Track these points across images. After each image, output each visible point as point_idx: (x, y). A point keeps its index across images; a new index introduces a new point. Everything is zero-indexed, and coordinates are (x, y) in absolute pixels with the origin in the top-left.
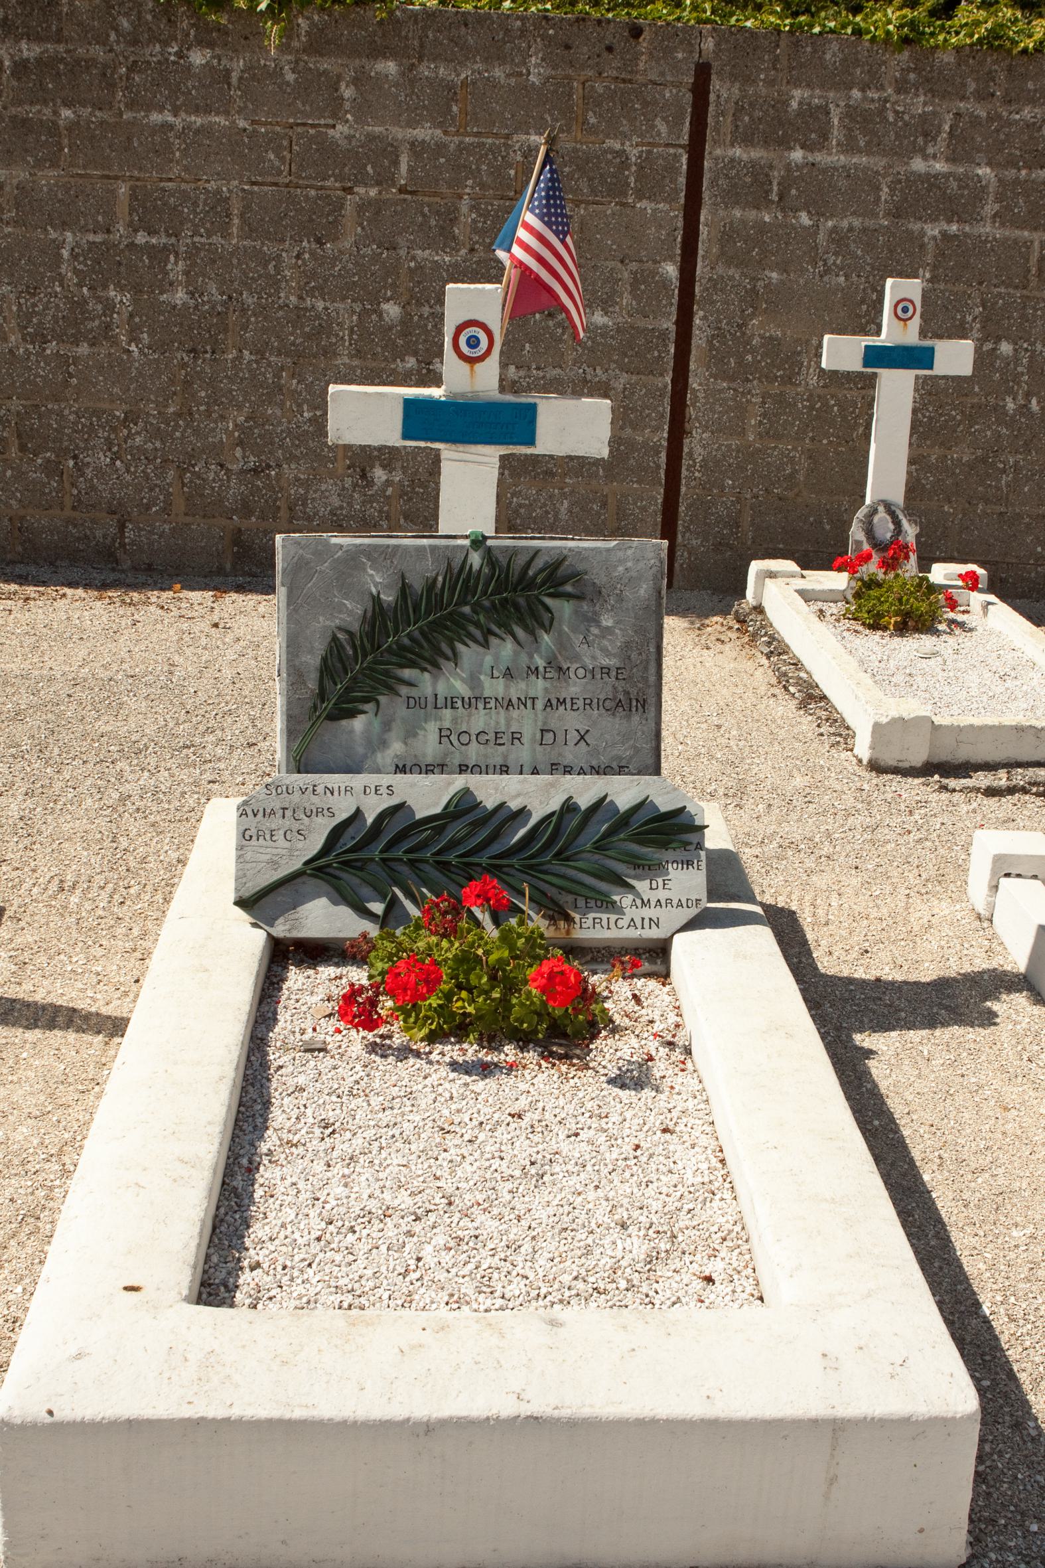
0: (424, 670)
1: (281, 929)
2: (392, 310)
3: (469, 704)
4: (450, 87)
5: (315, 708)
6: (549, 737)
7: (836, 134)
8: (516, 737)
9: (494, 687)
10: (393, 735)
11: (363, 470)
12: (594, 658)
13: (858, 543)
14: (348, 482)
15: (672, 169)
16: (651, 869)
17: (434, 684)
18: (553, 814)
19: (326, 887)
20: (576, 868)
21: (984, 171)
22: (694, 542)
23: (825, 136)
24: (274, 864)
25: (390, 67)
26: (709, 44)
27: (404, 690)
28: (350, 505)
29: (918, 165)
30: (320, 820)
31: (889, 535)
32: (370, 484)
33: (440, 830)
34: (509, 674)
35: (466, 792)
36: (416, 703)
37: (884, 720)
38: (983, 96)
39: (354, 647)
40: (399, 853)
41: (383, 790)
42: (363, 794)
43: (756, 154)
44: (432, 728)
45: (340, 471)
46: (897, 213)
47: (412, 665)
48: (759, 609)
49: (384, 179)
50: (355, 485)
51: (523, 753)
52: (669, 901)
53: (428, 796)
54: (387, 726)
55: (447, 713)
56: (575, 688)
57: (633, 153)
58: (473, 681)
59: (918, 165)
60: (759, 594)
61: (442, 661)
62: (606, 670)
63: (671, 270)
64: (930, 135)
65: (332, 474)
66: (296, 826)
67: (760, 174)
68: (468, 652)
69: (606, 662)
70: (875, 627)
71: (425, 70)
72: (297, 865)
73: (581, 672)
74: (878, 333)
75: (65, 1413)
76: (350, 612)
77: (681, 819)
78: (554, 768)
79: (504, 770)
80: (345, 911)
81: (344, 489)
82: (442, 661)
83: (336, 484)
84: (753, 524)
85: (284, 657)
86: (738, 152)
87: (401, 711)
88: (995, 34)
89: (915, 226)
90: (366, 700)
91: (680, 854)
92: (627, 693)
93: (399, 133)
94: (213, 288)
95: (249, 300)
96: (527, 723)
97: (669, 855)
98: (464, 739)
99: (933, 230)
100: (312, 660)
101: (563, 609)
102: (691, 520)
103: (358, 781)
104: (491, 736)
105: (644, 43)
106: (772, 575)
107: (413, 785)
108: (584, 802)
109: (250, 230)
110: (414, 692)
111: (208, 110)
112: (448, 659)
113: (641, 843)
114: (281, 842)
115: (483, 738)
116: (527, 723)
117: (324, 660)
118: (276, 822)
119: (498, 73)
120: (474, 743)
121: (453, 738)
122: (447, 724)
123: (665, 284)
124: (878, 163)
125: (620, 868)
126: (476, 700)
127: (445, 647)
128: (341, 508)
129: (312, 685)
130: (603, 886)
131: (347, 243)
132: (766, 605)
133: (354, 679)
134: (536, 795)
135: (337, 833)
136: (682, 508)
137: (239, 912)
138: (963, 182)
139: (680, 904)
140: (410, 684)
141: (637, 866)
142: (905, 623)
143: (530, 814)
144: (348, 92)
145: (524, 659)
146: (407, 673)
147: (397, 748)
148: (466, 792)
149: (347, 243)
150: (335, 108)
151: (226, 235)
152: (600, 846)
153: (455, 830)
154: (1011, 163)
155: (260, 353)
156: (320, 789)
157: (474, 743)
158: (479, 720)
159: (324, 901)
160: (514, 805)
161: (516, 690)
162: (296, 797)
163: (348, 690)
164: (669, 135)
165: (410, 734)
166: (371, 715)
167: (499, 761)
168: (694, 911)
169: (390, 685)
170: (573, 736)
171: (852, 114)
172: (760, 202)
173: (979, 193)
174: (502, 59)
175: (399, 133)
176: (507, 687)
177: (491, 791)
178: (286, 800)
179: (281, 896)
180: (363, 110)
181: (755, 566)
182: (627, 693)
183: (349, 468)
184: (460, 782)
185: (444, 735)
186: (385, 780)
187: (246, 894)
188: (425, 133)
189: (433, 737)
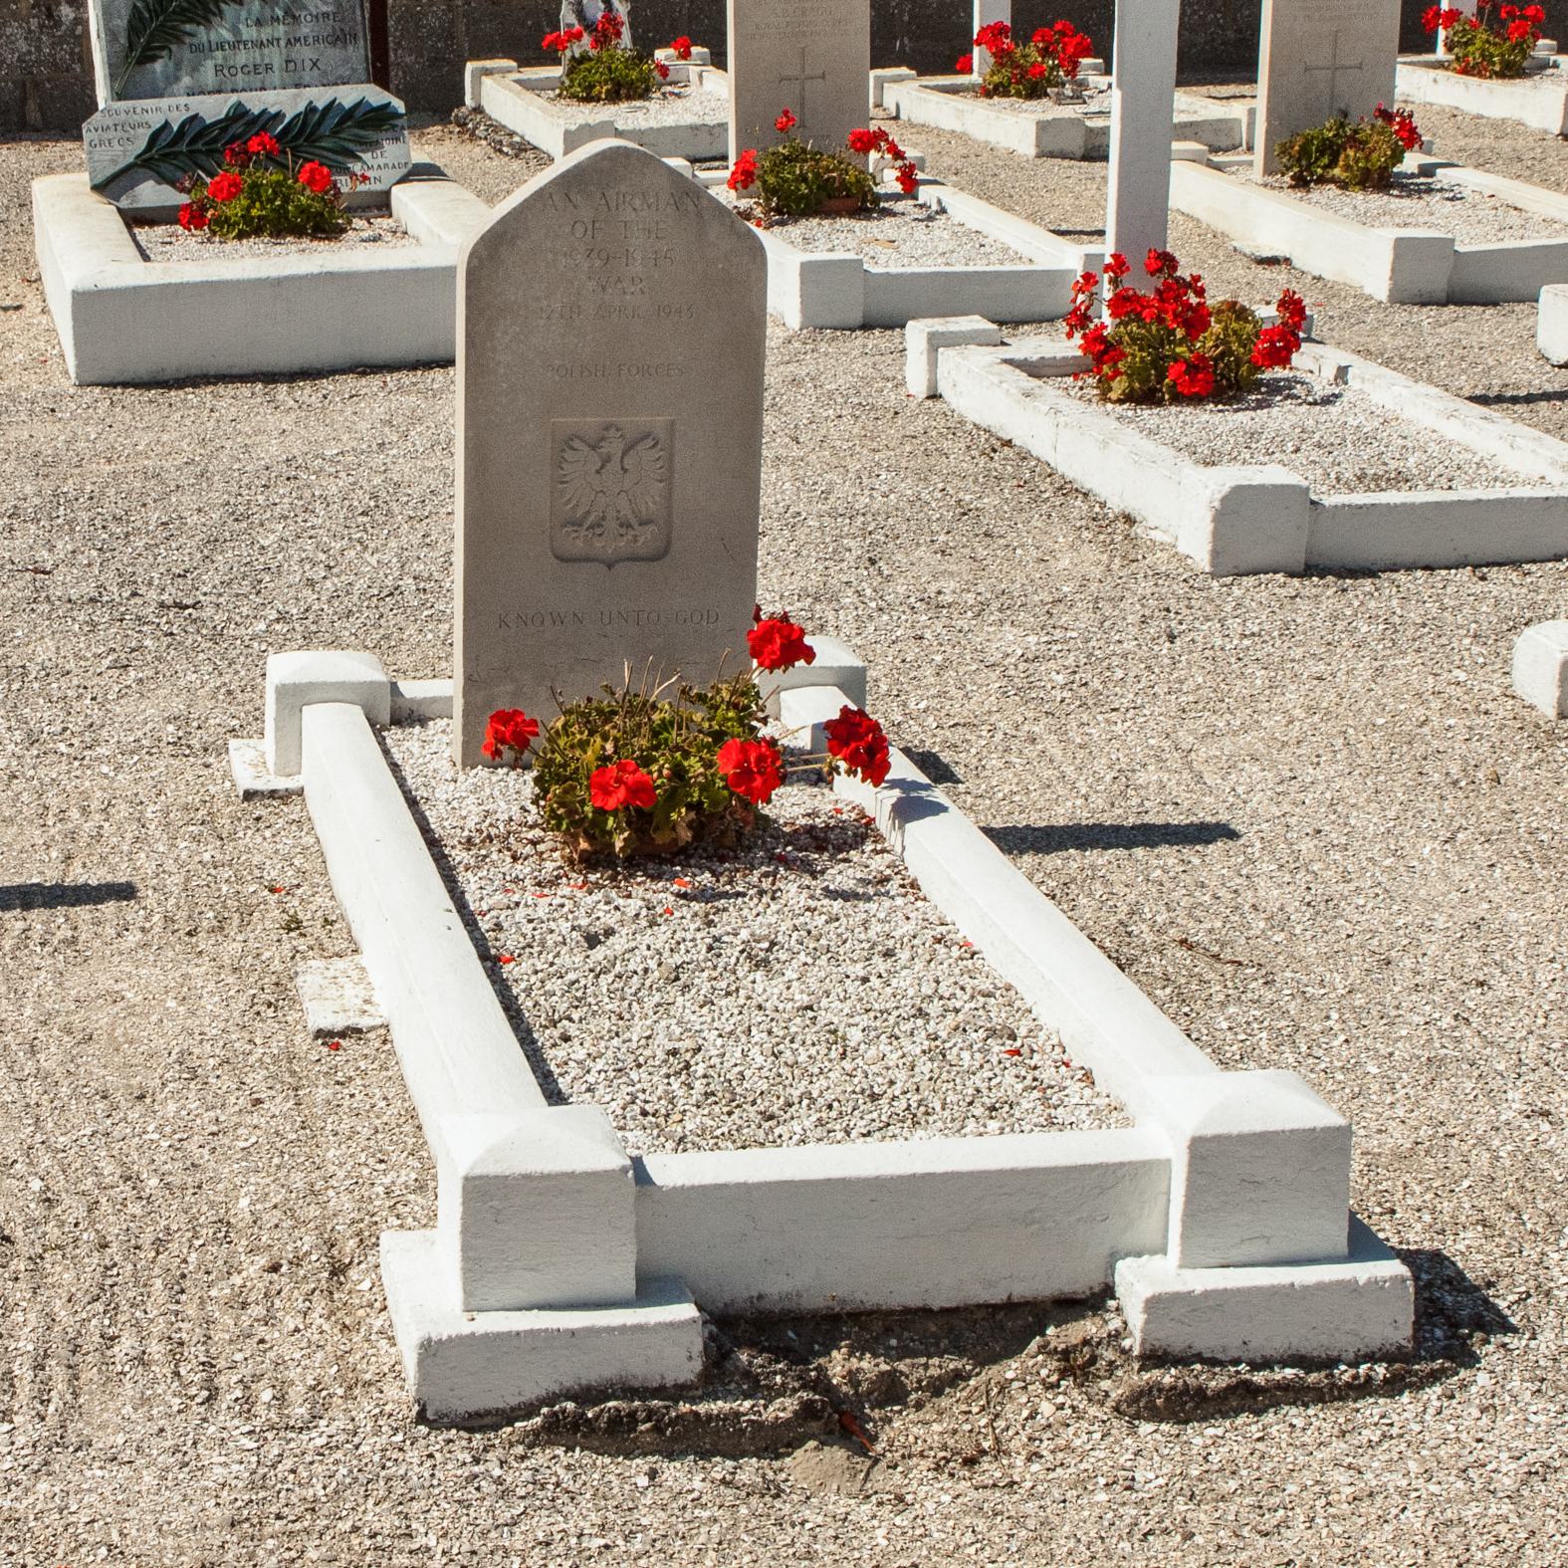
0: (199, 24)
1: (124, 203)
3: (234, 46)
5: (127, 57)
6: (291, 66)
8: (269, 68)
9: (249, 33)
10: (183, 72)
11: (49, 9)
12: (317, 7)
13: (569, 25)
14: (34, 23)
16: (373, 145)
17: (208, 34)
18: (299, 115)
19: (151, 173)
20: (323, 148)
22: (408, 60)
24: (114, 161)
27: (188, 40)
28: (39, 49)
30: (141, 130)
31: (600, 15)
32: (58, 23)
33: (224, 130)
34: (259, 23)
35: (239, 104)
36: (198, 49)
37: (573, 128)
39: (149, 11)
40: (199, 146)
41: (182, 107)
42: (169, 110)
44: (210, 64)
45: (24, 12)
47: (191, 21)
48: (478, 110)
50: (41, 26)
51: (276, 77)
52: (386, 165)
53: (213, 108)
54: (178, 66)
55: (219, 54)
56: (305, 30)
58: (235, 30)
60: (477, 95)
61: (212, 18)
62: (326, 15)
65: (15, 16)
66: (126, 135)
69: (325, 9)
70: (588, 99)
72: (131, 160)
73: (309, 18)
74: (970, 71)
75: (102, 285)
77: (389, 110)
78: (297, 86)
79: (263, 89)
80: (166, 188)
81: (30, 31)
82: (212, 18)
83: (21, 26)
84: (467, 34)
85: (101, 22)
87: (187, 55)
90: (162, 48)
91: (390, 134)
92: (342, 30)
96: (275, 56)
97: (383, 135)
98: (233, 71)
100: (121, 23)
102: (402, 35)
103: (164, 103)
104: (251, 68)
106: (488, 72)
107: (202, 102)
108: (320, 105)
110: (195, 41)
112: (214, 14)
113: (362, 128)
114: (117, 147)
115: (246, 70)
117: (129, 22)
118: (111, 134)
120: (240, 74)
121: (225, 71)
122: (220, 62)
125: (351, 146)
126: (238, 43)
127: (212, 6)
128: (29, 52)
129: (123, 40)
130: (340, 158)
132: (485, 103)
133: (151, 34)
134: (284, 102)
135: (154, 138)
136: (391, 23)
137: (95, 197)
139: (394, 166)
140: (190, 35)
141: (361, 144)
142: (617, 93)
143: (284, 116)
145: (268, 12)
146: (188, 27)
147: (186, 80)
148: (239, 104)
152: (335, 133)
153: (237, 128)
156: (138, 110)
157: (240, 74)
158: (242, 57)
159: (151, 183)
160: (273, 110)
161: (266, 33)
162: (123, 116)
163: (148, 42)
165: (195, 69)
166: (166, 59)
167: (259, 85)
168: (404, 171)
170: (308, 64)
176: (258, 31)
177: (257, 102)
178: (116, 119)
179: (123, 181)
181: (470, 66)
182: (342, 30)
183: (33, 7)
184: (234, 98)
185: (218, 69)
186: (183, 100)
187: (100, 178)
189: (211, 72)
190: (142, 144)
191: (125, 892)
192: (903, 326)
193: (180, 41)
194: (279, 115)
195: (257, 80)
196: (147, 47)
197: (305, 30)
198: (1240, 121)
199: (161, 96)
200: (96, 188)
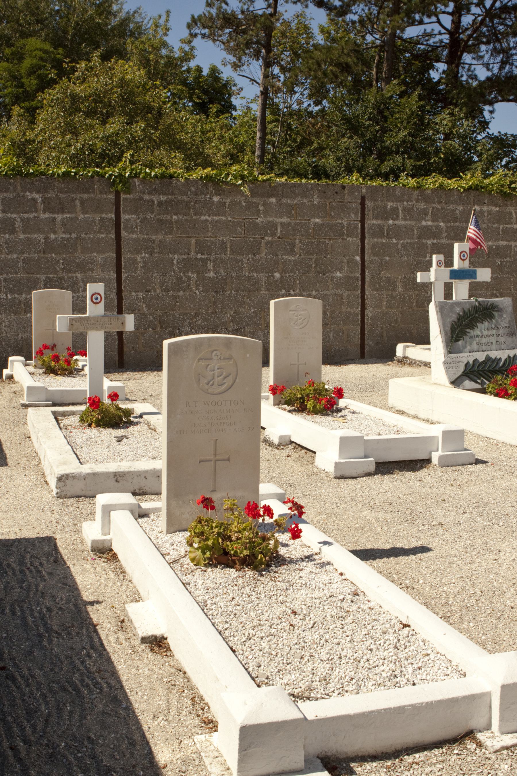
2: (277, 275)
4: (292, 206)
7: (401, 215)
9: (485, 332)
15: (356, 227)
21: (442, 224)
23: (398, 216)
24: (455, 374)
25: (273, 200)
26: (364, 190)
29: (424, 223)
34: (488, 329)
36: (471, 337)
38: (439, 202)
42: (467, 357)
43: (379, 222)
44: (475, 342)
46: (419, 238)
49: (273, 235)
51: (494, 347)
53: (481, 357)
54: (466, 343)
56: (501, 331)
57: (345, 223)
59: (424, 223)
62: (506, 327)
63: (358, 258)
64: (426, 214)
67: (381, 228)
68: (479, 325)
71: (284, 201)
76: (454, 317)
80: (472, 383)
86: (374, 222)
87: (468, 339)
88: (441, 185)
89: (425, 241)
93: (278, 220)
94: (222, 271)
95: (234, 274)
99: (429, 242)
100: (448, 329)
101: (496, 314)
105: (346, 191)
109: (233, 252)
111: (219, 215)
116: (493, 340)
119: (305, 201)
123: (356, 262)
124: (413, 223)
126: (482, 336)
131: (263, 255)
134: (502, 355)
138: (437, 227)
144: (261, 208)
146: (468, 330)
147: (469, 347)
149: (263, 255)
150: (258, 213)
151: (225, 252)
154: (449, 221)
155: (237, 291)
158: (484, 340)
160: (498, 357)
161: (490, 332)
164: (355, 217)
165: (471, 344)
169: (465, 333)
170: (503, 343)
171: (405, 209)
172: (382, 236)
173: (441, 230)
174: (306, 197)
175: (278, 220)
177: (494, 354)
180: (266, 213)
184: (486, 353)
185: (478, 344)
188: (285, 220)
189: (475, 345)
190: (462, 369)
191: (424, 549)
192: (95, 497)
193: (466, 335)
194: (500, 359)
195: (489, 348)
196: (457, 336)
197: (501, 331)
198: (438, 437)
199: (461, 353)
200: (452, 383)
